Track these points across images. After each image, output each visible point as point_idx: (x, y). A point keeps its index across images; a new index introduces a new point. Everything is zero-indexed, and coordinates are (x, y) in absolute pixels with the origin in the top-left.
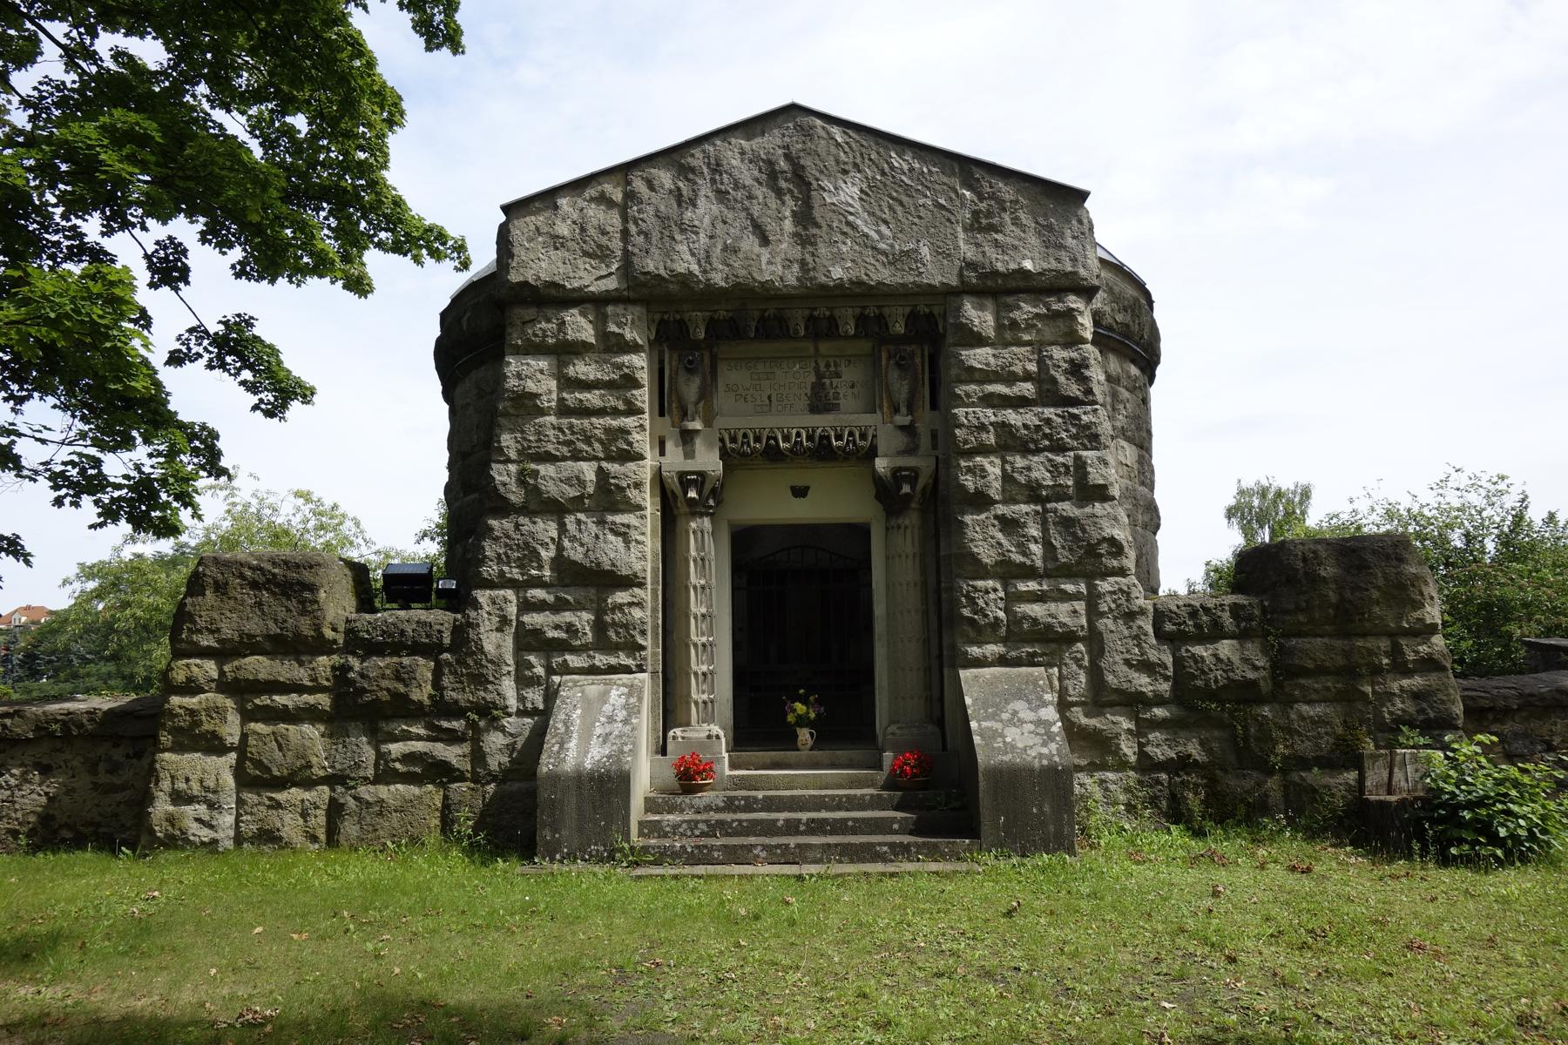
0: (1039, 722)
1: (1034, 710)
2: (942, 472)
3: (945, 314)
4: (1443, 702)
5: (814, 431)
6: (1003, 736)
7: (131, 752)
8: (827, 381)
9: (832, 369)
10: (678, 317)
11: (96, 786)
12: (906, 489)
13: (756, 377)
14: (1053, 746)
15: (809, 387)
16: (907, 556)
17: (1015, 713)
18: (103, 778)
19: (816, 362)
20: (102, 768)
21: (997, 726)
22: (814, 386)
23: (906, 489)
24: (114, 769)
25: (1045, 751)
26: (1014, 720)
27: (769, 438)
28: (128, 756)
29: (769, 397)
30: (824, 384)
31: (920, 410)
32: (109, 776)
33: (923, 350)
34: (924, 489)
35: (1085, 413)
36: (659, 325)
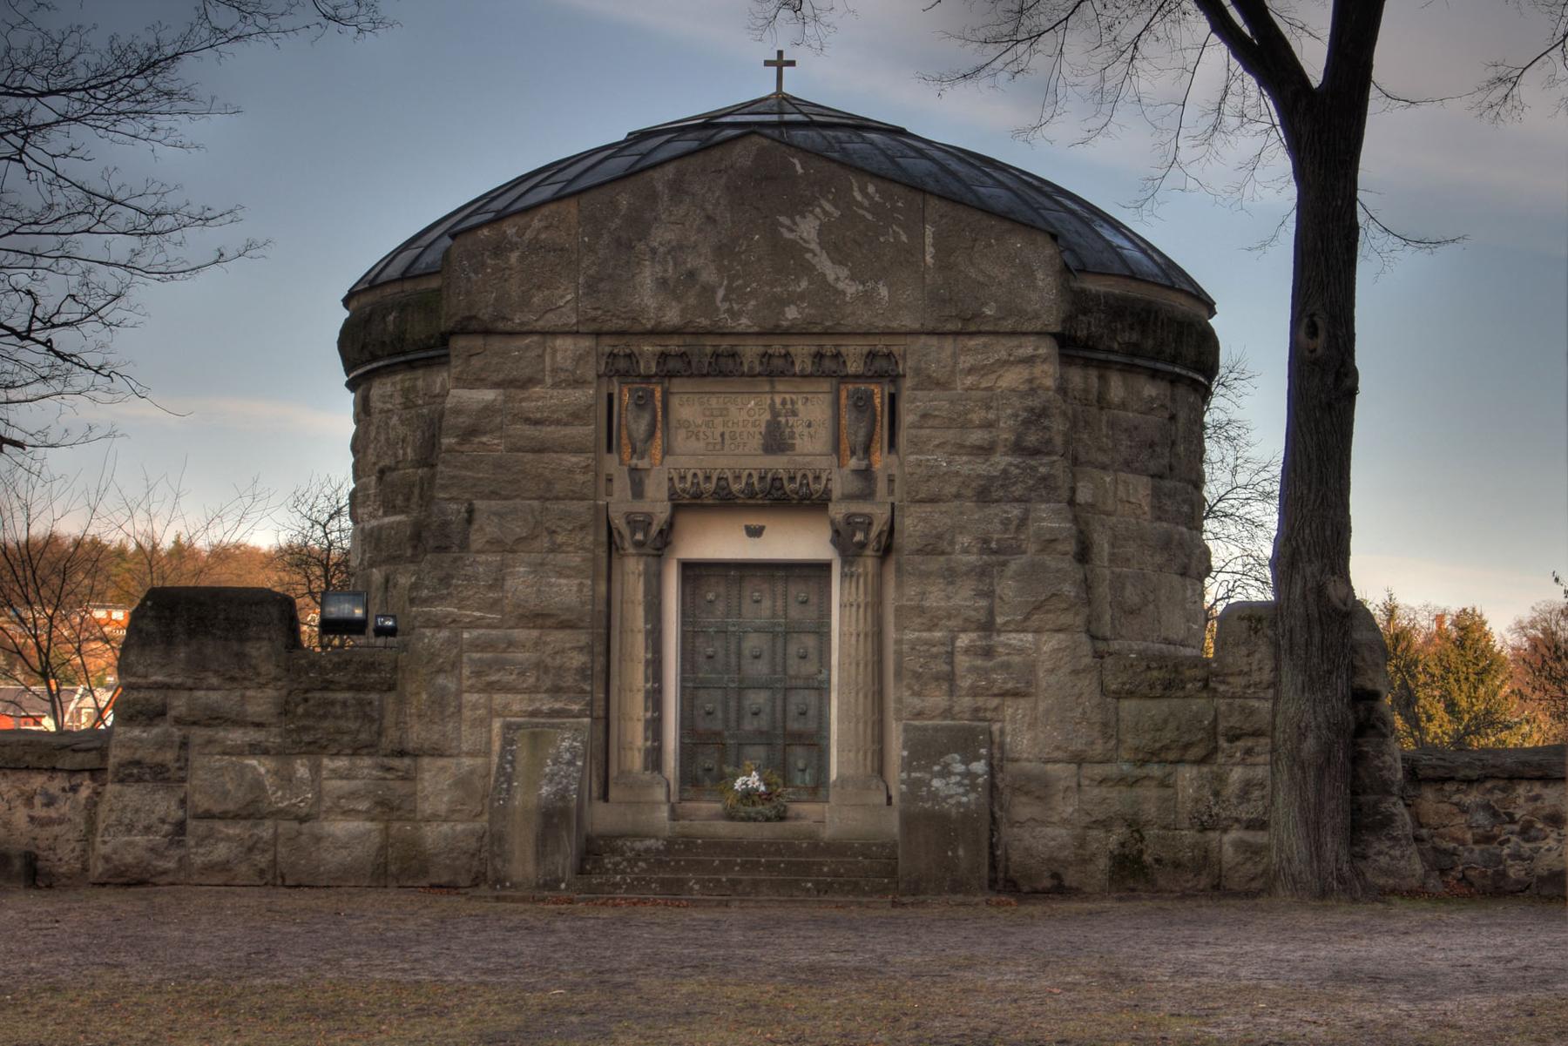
0: (969, 774)
1: (966, 762)
2: (897, 520)
3: (905, 354)
4: (1381, 770)
5: (766, 473)
6: (929, 785)
7: (67, 785)
8: (783, 420)
9: (789, 406)
10: (628, 351)
11: (32, 819)
12: (859, 537)
13: (708, 413)
14: (973, 796)
15: (763, 425)
16: (859, 606)
17: (947, 765)
18: (39, 811)
19: (772, 400)
20: (38, 801)
21: (928, 776)
22: (769, 424)
23: (859, 537)
24: (50, 802)
25: (964, 799)
26: (946, 773)
27: (719, 479)
28: (64, 790)
29: (722, 435)
30: (779, 422)
31: (878, 454)
32: (45, 809)
33: (883, 390)
34: (879, 535)
35: (1041, 465)
36: (609, 357)
